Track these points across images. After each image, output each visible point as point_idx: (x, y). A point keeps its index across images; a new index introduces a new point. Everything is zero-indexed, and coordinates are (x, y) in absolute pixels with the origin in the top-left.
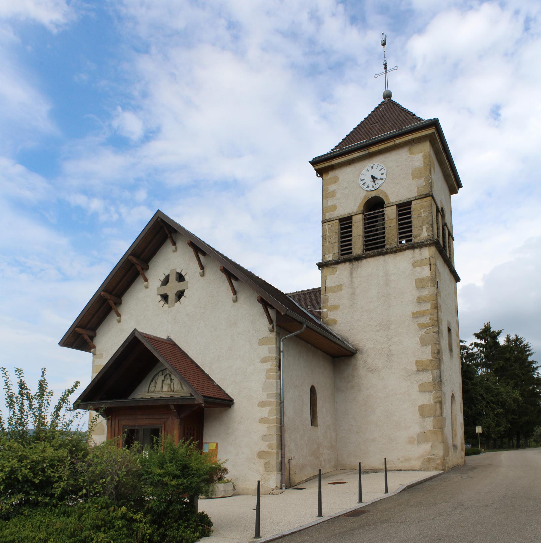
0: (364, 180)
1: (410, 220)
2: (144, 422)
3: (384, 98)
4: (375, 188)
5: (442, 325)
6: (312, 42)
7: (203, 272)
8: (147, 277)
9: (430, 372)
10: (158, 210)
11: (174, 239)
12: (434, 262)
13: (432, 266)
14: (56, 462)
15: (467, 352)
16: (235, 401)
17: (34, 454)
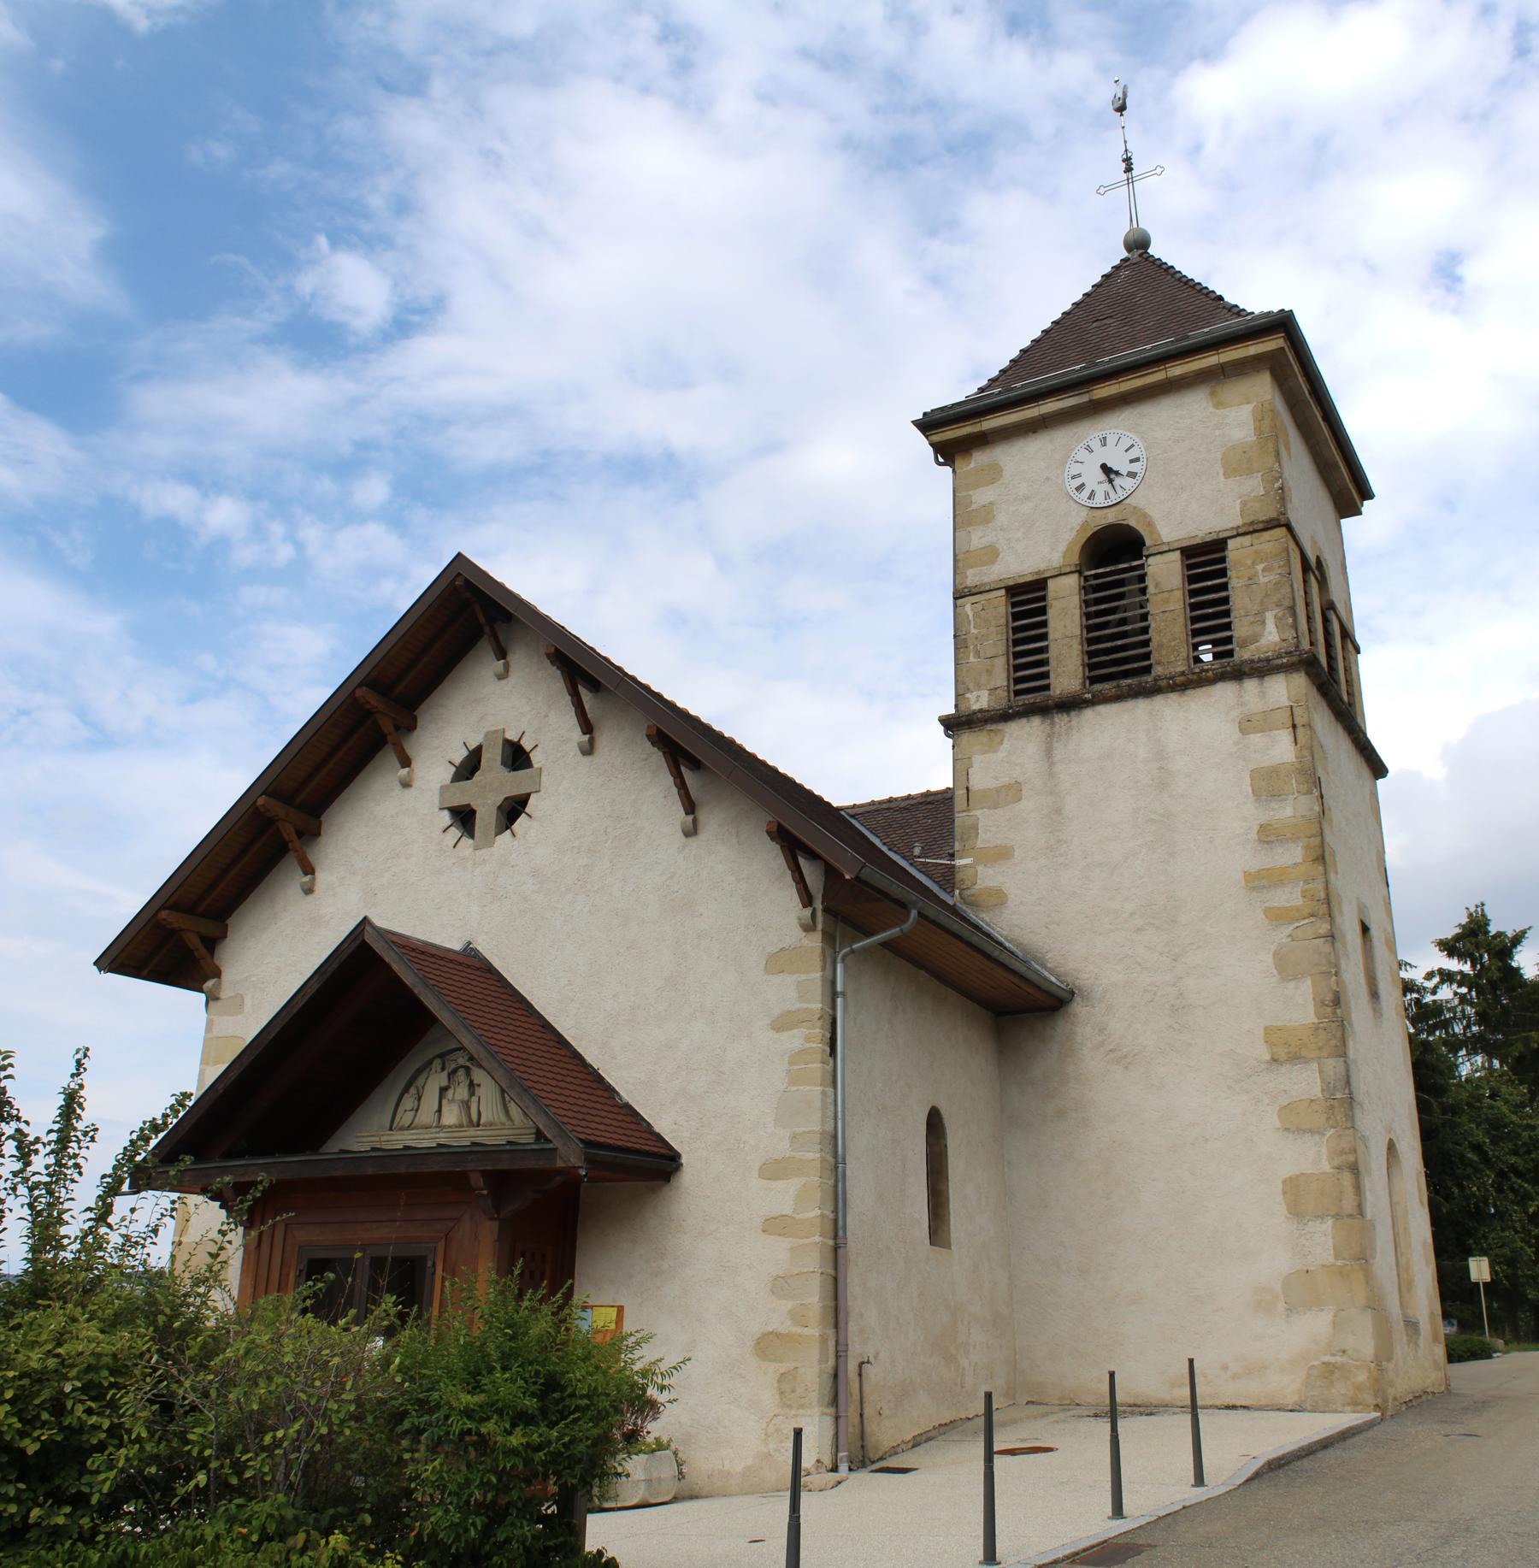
0: (1079, 475)
1: (1224, 594)
2: (377, 1232)
3: (1129, 247)
4: (1114, 499)
5: (1341, 912)
6: (895, 78)
7: (592, 742)
8: (408, 752)
9: (1315, 1065)
10: (459, 554)
11: (501, 638)
12: (1304, 720)
13: (1300, 731)
14: (105, 1373)
15: (1418, 1001)
16: (684, 1160)
17: (33, 1345)
